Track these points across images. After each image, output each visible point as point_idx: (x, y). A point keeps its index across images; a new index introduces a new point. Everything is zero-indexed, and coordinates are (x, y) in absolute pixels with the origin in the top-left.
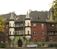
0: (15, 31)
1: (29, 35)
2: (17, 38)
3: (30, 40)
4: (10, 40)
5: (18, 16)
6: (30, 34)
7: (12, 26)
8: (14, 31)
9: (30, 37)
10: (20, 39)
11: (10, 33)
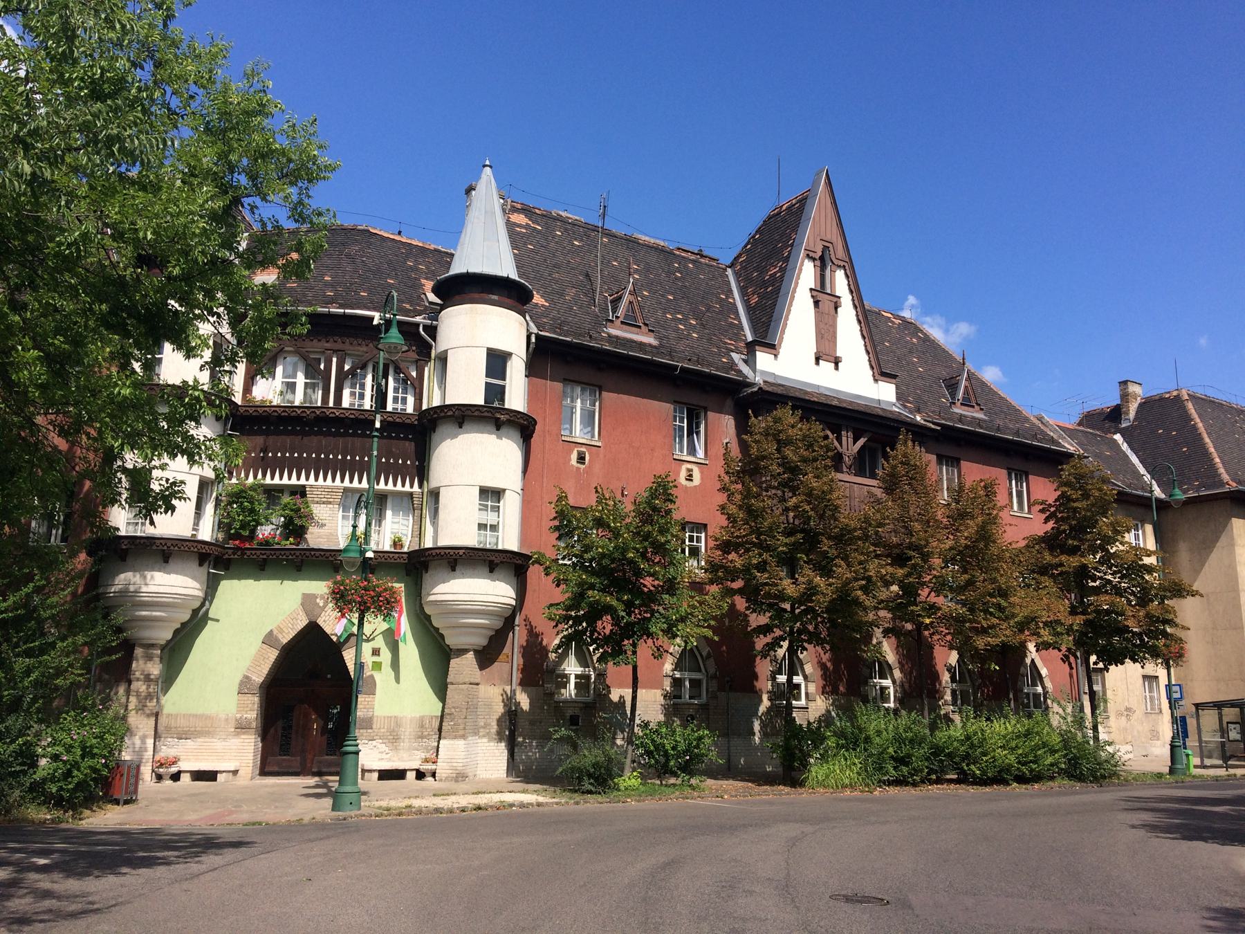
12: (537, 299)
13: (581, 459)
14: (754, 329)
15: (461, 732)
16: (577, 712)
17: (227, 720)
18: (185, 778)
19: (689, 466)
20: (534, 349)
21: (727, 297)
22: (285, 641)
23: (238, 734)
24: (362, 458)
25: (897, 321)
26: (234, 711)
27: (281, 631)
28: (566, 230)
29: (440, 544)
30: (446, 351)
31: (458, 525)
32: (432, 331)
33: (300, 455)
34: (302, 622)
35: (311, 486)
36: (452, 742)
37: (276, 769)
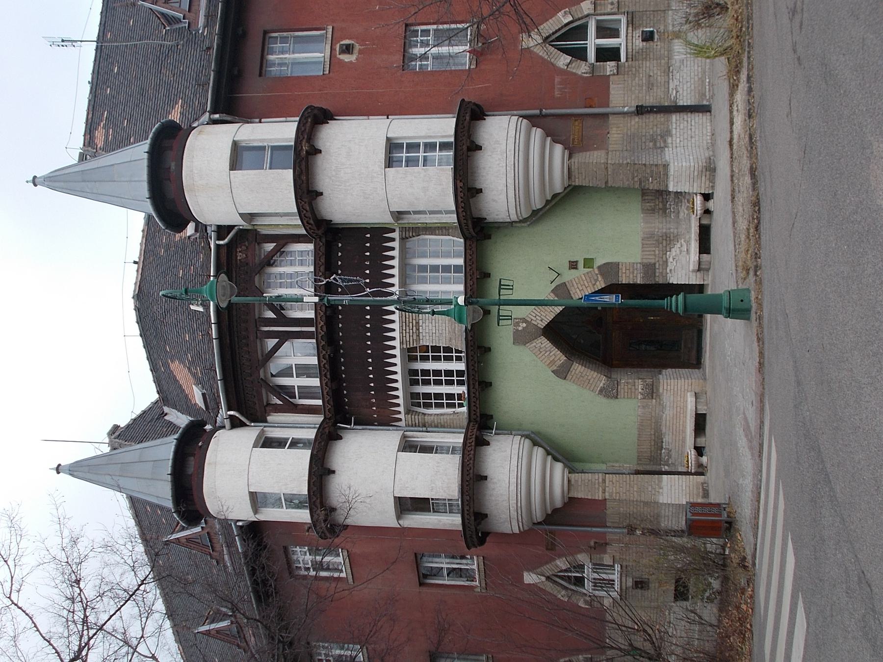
0: (386, 421)
1: (465, 150)
2: (529, 376)
3: (568, 118)
4: (566, 522)
5: (158, 381)
6: (502, 298)
7: (289, 471)
8: (389, 439)
9: (501, 134)
10: (554, 332)
11: (421, 505)
12: (175, 116)
13: (348, 49)
15: (661, 169)
16: (638, 33)
17: (644, 407)
18: (701, 442)
20: (228, 113)
22: (564, 358)
23: (659, 396)
24: (368, 312)
26: (635, 401)
27: (553, 362)
28: (104, 83)
29: (454, 208)
30: (242, 215)
31: (429, 189)
32: (222, 231)
33: (369, 356)
34: (544, 343)
35: (402, 343)
36: (671, 178)
37: (694, 352)
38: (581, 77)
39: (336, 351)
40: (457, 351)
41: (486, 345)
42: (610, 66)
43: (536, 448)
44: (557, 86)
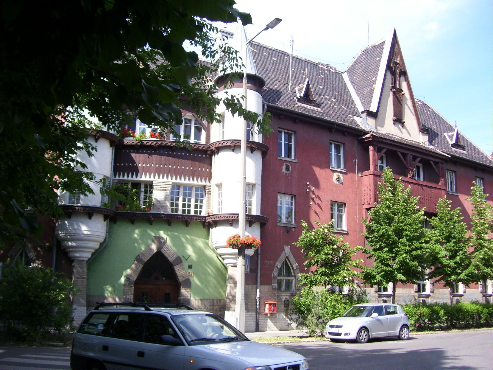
4: (61, 257)
13: (287, 168)
14: (363, 104)
19: (338, 174)
21: (133, 164)
22: (145, 260)
25: (420, 103)
35: (156, 181)
38: (272, 272)
39: (189, 152)
40: (201, 212)
41: (233, 225)
42: (276, 285)
43: (99, 244)
44: (269, 262)
